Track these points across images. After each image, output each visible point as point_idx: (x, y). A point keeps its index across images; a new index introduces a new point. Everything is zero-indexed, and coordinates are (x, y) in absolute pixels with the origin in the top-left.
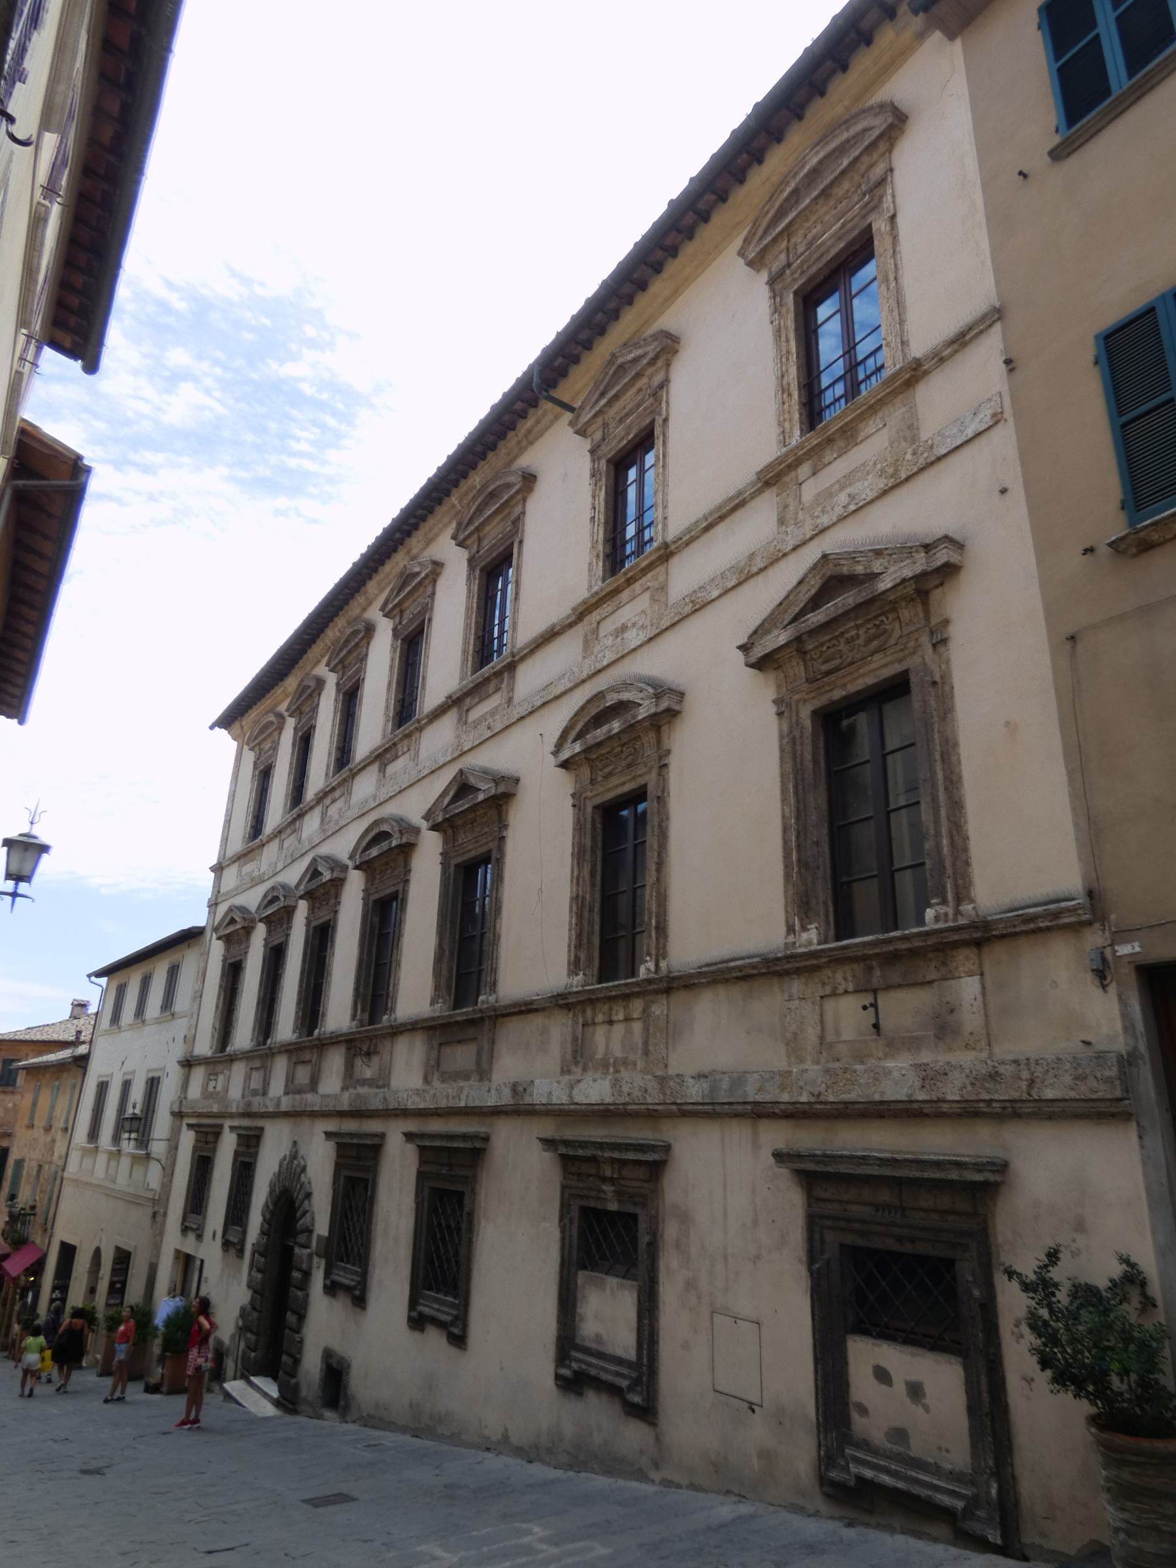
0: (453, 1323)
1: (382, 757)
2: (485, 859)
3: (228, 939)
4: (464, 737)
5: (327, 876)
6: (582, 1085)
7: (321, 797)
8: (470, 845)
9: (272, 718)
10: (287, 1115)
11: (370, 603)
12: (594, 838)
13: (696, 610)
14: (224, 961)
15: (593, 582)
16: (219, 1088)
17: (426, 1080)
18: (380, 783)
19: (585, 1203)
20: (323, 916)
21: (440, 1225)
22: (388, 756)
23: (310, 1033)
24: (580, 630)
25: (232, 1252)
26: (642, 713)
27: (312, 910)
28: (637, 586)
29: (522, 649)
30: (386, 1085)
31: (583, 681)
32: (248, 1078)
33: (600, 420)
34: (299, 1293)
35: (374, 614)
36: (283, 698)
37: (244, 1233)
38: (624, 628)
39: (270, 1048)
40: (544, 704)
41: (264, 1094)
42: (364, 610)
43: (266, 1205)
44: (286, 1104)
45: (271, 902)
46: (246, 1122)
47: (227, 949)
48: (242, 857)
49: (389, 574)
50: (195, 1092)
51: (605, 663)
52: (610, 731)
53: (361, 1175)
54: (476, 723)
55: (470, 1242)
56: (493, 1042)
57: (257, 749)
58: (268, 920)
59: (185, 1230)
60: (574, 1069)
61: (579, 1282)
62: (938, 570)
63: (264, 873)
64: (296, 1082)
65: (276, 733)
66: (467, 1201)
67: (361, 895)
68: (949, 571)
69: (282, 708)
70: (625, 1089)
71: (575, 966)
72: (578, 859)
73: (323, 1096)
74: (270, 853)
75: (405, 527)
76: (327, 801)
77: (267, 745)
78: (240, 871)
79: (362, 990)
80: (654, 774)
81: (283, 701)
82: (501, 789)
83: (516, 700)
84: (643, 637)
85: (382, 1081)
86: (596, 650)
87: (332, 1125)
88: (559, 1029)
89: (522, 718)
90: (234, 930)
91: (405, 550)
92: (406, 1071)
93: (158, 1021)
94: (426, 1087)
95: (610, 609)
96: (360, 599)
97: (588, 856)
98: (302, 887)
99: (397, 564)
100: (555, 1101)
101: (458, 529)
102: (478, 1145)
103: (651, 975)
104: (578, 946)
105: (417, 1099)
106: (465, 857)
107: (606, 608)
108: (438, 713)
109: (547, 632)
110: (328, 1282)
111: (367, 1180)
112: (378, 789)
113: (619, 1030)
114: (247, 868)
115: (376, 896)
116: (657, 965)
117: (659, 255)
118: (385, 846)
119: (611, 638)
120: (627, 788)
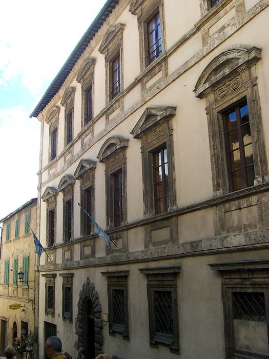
0: (172, 345)
1: (106, 112)
2: (163, 147)
3: (47, 201)
4: (145, 95)
5: (88, 167)
6: (228, 239)
7: (80, 136)
8: (154, 140)
9: (55, 109)
10: (83, 267)
11: (93, 50)
12: (219, 127)
13: (263, 10)
14: (47, 210)
15: (203, 12)
16: (52, 260)
17: (146, 246)
18: (107, 124)
19: (234, 290)
20: (88, 185)
21: (160, 306)
22: (109, 112)
23: (89, 233)
24: (199, 34)
25: (68, 321)
26: (241, 62)
27: (82, 184)
28: (228, 7)
29: (169, 51)
30: (127, 250)
31: (204, 57)
32: (64, 255)
33: (106, 49)
34: (99, 336)
35: (96, 54)
36: (58, 100)
37: (72, 314)
38: (223, 28)
39: (72, 242)
40: (184, 72)
41: (72, 260)
42: (90, 54)
43: (79, 303)
44: (82, 263)
45: (64, 183)
46: (65, 272)
47: (48, 205)
48: (49, 167)
49: (100, 35)
50: (43, 262)
51: (215, 45)
52: (224, 74)
53: (120, 288)
54: (151, 88)
55: (177, 311)
56: (177, 226)
57: (64, 105)
58: (63, 191)
59: (47, 314)
60: (222, 232)
61: (235, 324)
62: (170, 114)
63: (59, 172)
64: (85, 254)
65: (57, 114)
66: (173, 294)
67: (80, 188)
68: (171, 116)
69: (59, 104)
70: (253, 237)
71: (217, 186)
72: (213, 137)
73: (98, 258)
74: (61, 163)
75: (78, 53)
76: (83, 137)
77: (54, 120)
78: (49, 173)
79: (110, 213)
80: (249, 90)
81: (59, 101)
82: (168, 113)
83: (170, 73)
84: (234, 29)
85: (125, 248)
86: (209, 41)
87: (104, 269)
88: (210, 215)
89: (174, 80)
90: (50, 196)
91: (107, 23)
92: (136, 242)
93: (14, 240)
94: (146, 249)
95: (214, 21)
96: (88, 49)
97: (218, 135)
98: (77, 174)
99: (104, 30)
100: (214, 247)
101: (131, 7)
102: (176, 271)
103: (261, 184)
104: (218, 177)
105: (143, 255)
106: (153, 148)
107: (212, 21)
108: (99, 117)
109: (182, 39)
110: (111, 332)
111: (123, 291)
112: (106, 126)
113: (245, 212)
114: (52, 171)
115: (111, 172)
116: (263, 179)
117: (101, 21)
118: (114, 149)
119: (217, 34)
120: (235, 100)
